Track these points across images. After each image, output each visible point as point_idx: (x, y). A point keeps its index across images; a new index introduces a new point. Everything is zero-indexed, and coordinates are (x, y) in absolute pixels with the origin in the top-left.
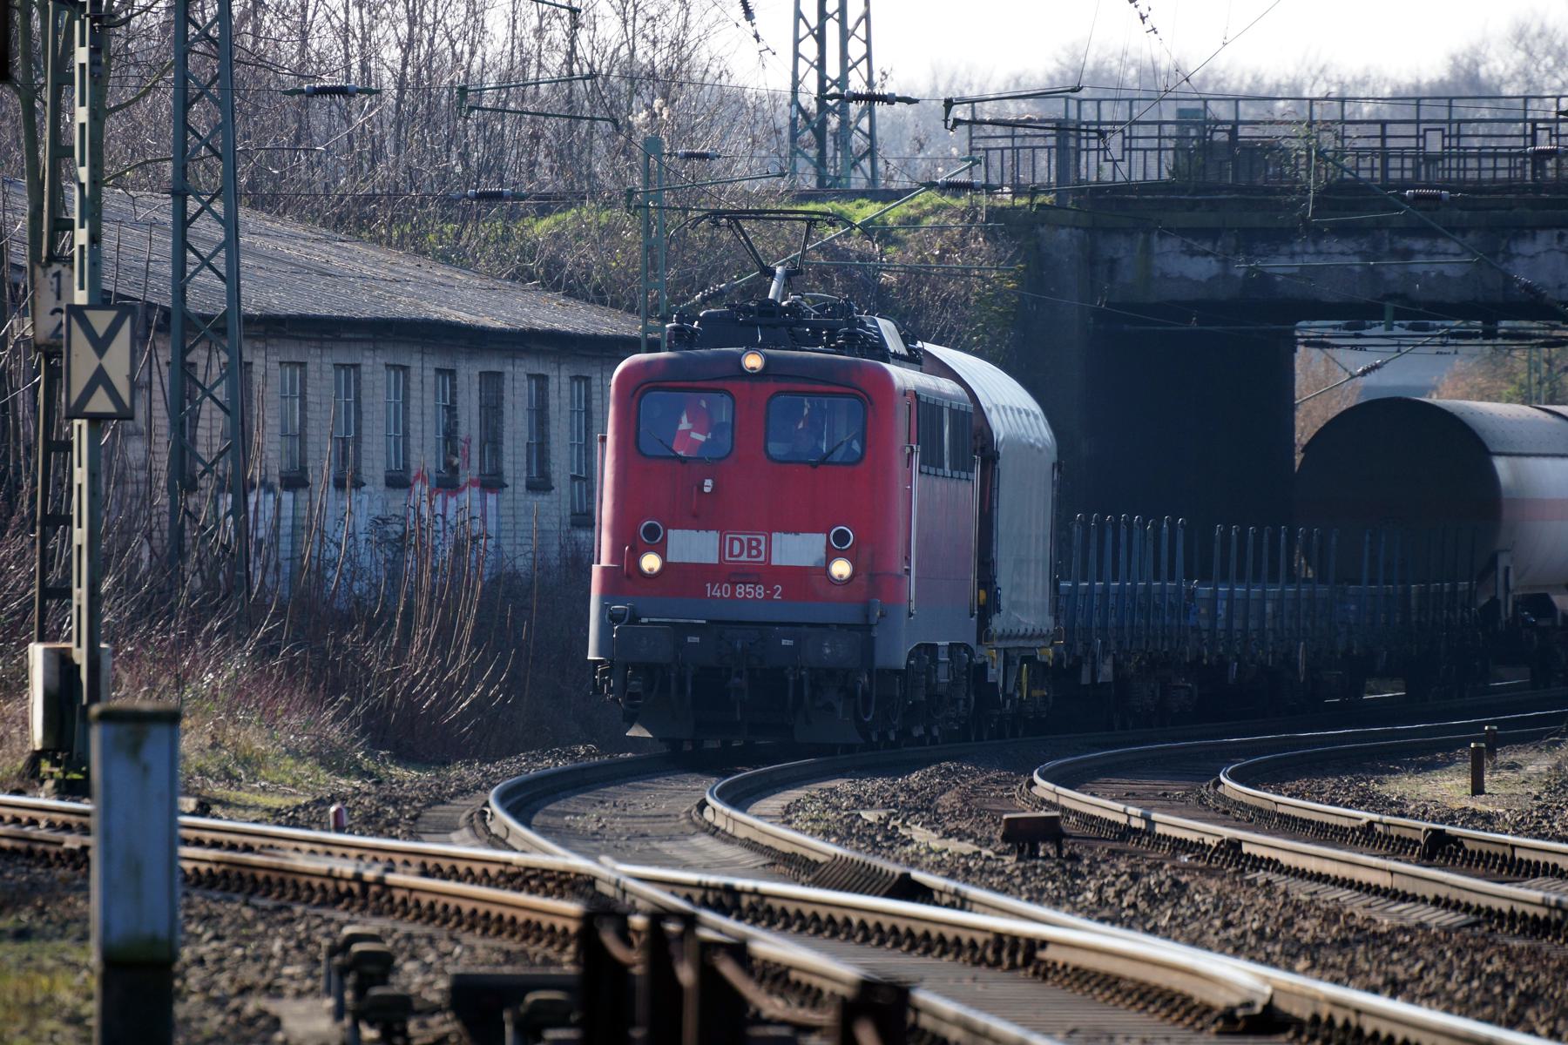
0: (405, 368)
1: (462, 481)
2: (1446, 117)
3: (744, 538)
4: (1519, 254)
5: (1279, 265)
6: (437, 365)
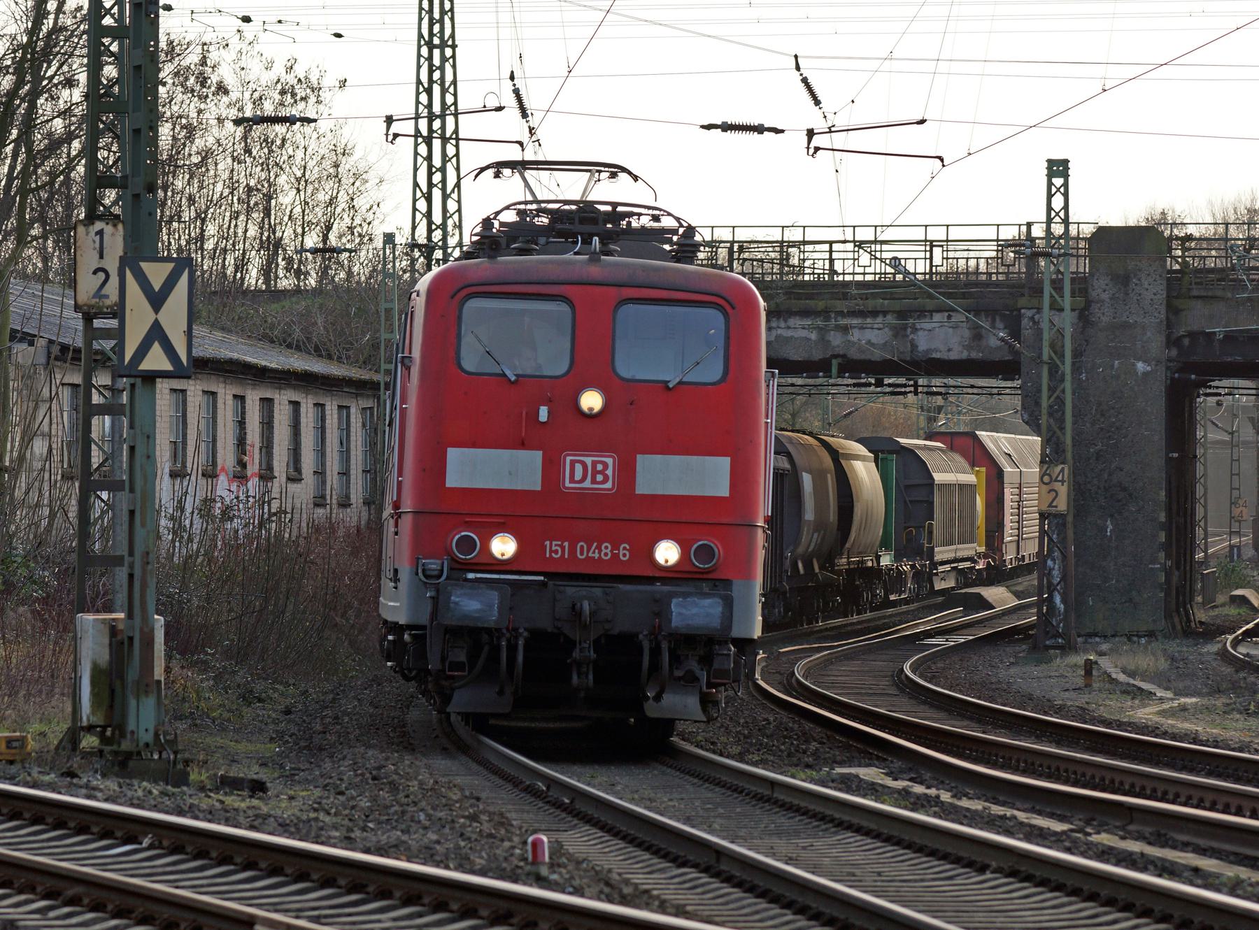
0: (214, 394)
1: (249, 474)
3: (588, 460)
6: (234, 392)
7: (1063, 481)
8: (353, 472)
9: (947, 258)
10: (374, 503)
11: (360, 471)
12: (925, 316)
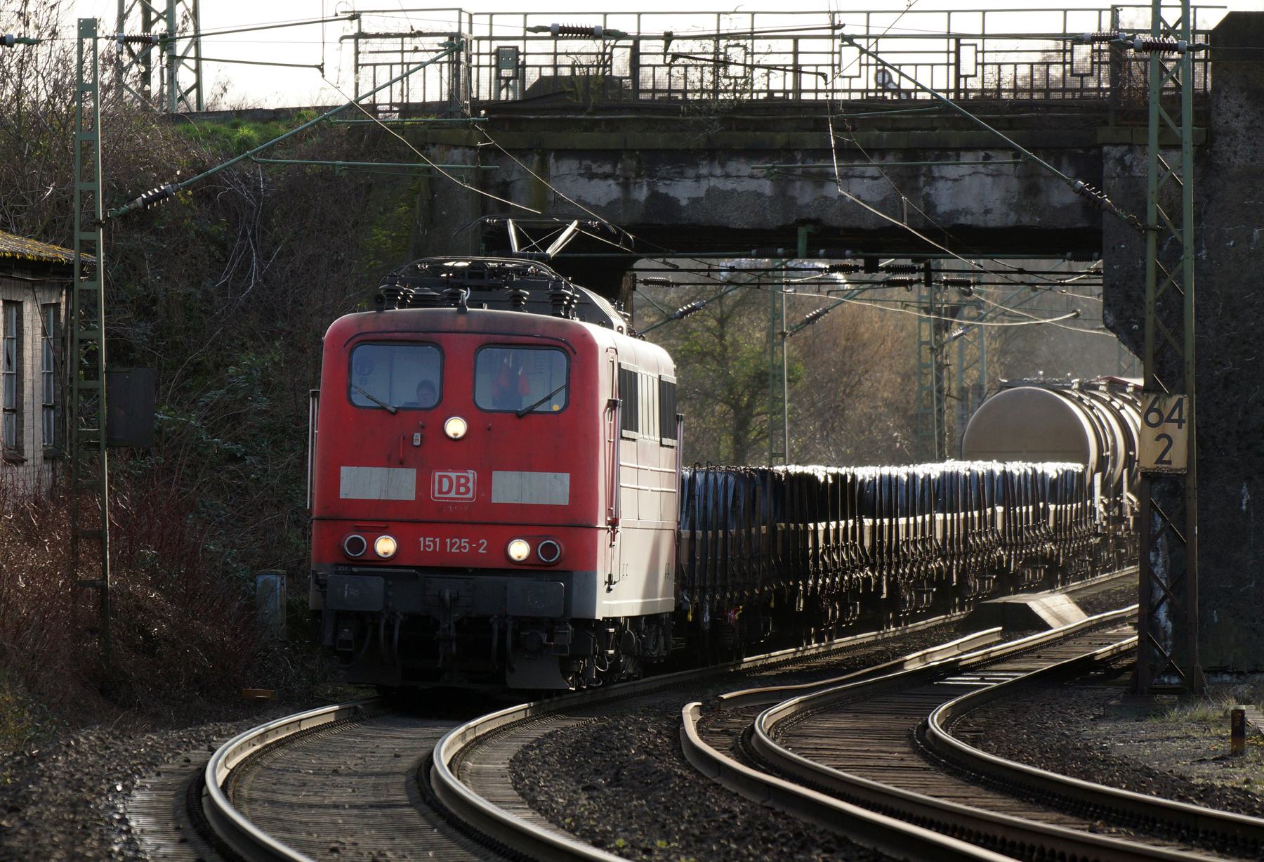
2: (864, 33)
3: (453, 475)
4: (942, 178)
5: (683, 191)
7: (1180, 422)
8: (27, 408)
9: (983, 64)
10: (61, 457)
11: (39, 406)
12: (948, 158)
